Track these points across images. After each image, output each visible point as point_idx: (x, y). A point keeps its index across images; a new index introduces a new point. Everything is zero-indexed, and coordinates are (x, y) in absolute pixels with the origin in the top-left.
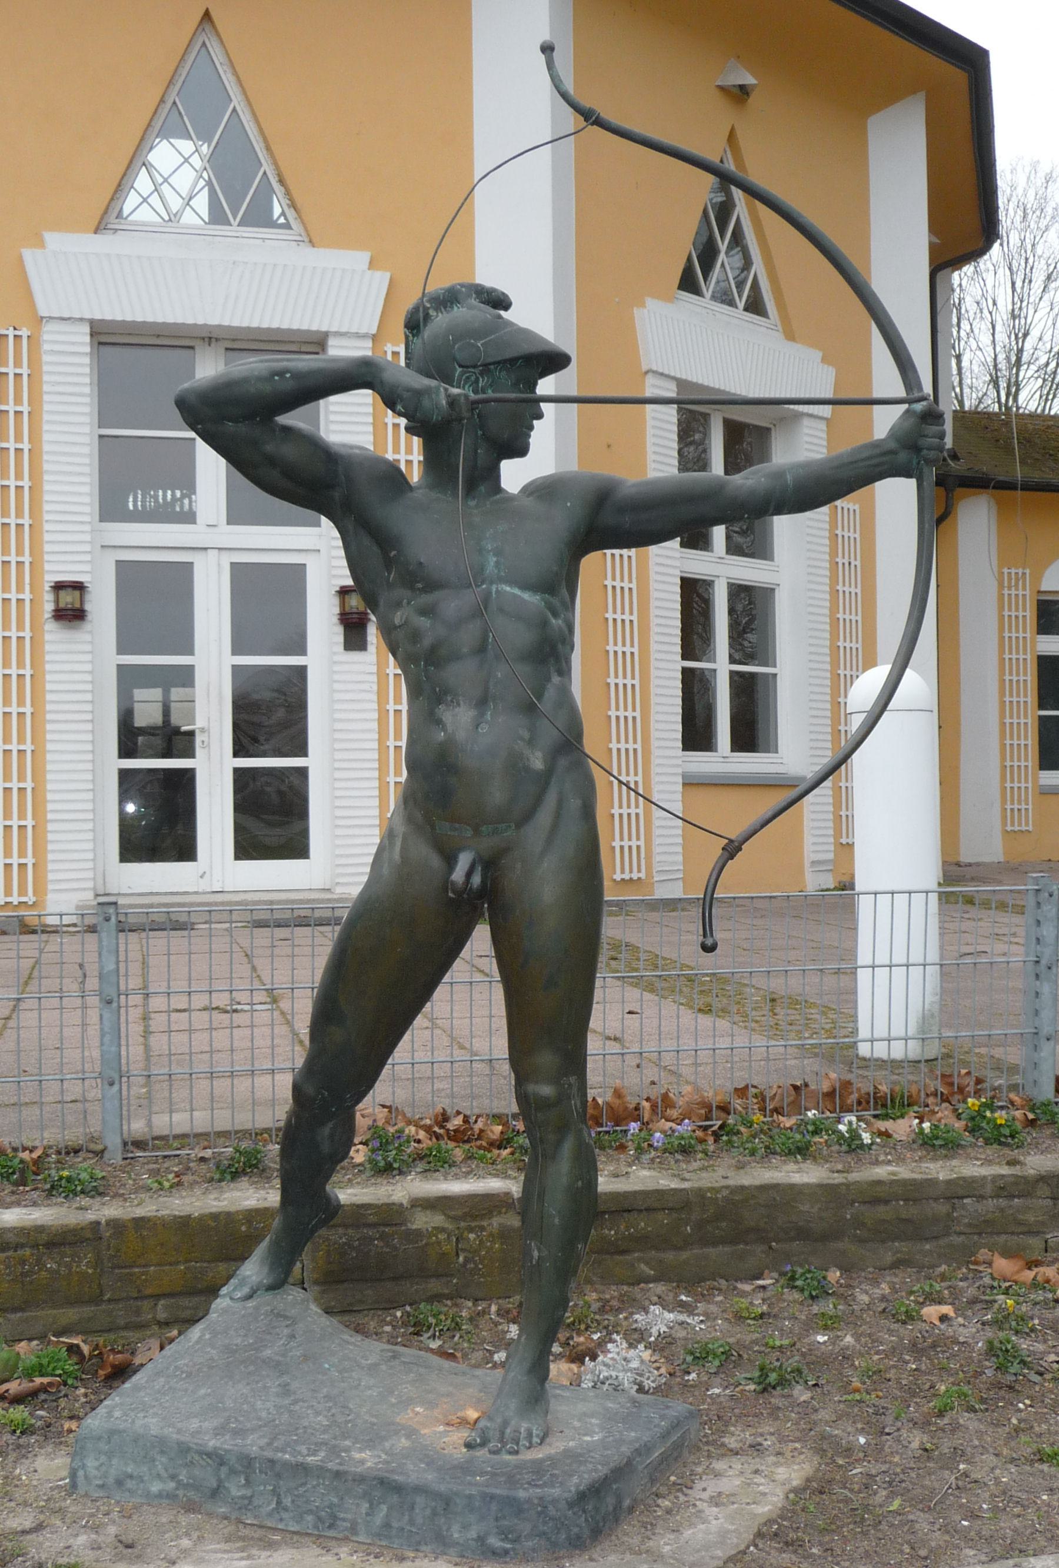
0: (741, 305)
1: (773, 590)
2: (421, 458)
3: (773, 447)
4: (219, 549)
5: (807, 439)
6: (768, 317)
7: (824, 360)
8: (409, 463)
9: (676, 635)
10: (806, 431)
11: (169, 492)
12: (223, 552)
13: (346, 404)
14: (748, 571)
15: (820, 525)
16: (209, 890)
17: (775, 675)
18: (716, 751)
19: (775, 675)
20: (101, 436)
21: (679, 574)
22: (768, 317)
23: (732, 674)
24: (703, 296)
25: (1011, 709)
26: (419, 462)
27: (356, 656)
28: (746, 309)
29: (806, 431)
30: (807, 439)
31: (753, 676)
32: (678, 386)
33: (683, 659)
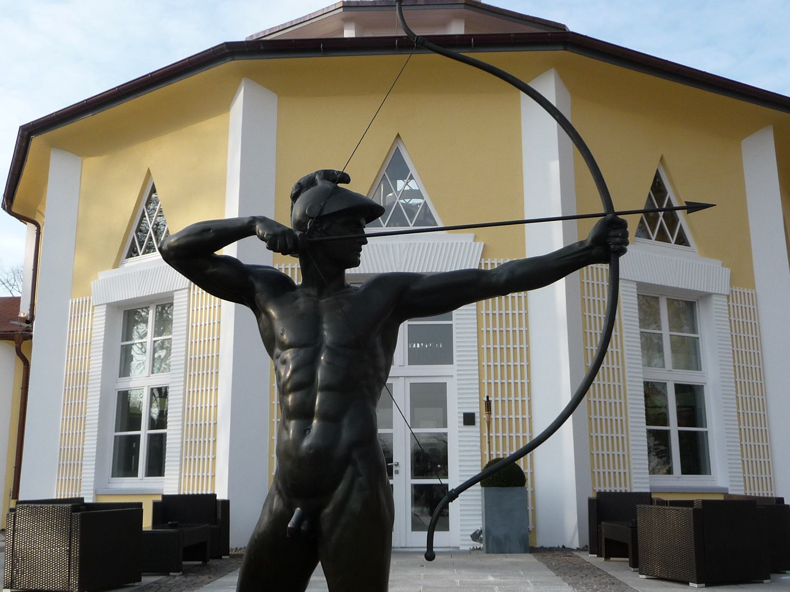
0: (673, 241)
1: (703, 386)
2: (608, 284)
3: (697, 309)
4: (404, 377)
5: (715, 306)
6: (690, 246)
7: (723, 265)
8: (293, 269)
9: (642, 413)
10: (715, 302)
11: (418, 344)
12: (406, 378)
13: (470, 310)
14: (688, 377)
15: (728, 351)
16: (399, 546)
17: (707, 432)
18: (673, 474)
19: (707, 432)
20: (670, 335)
21: (643, 380)
22: (690, 246)
23: (680, 432)
24: (651, 239)
25: (514, 337)
26: (600, 334)
27: (469, 428)
28: (676, 243)
29: (715, 302)
30: (715, 306)
31: (695, 432)
32: (637, 285)
33: (647, 425)
